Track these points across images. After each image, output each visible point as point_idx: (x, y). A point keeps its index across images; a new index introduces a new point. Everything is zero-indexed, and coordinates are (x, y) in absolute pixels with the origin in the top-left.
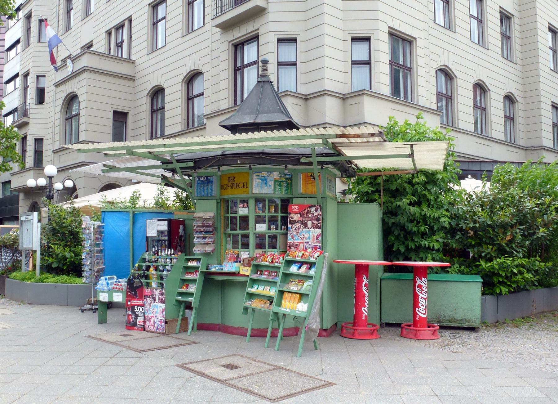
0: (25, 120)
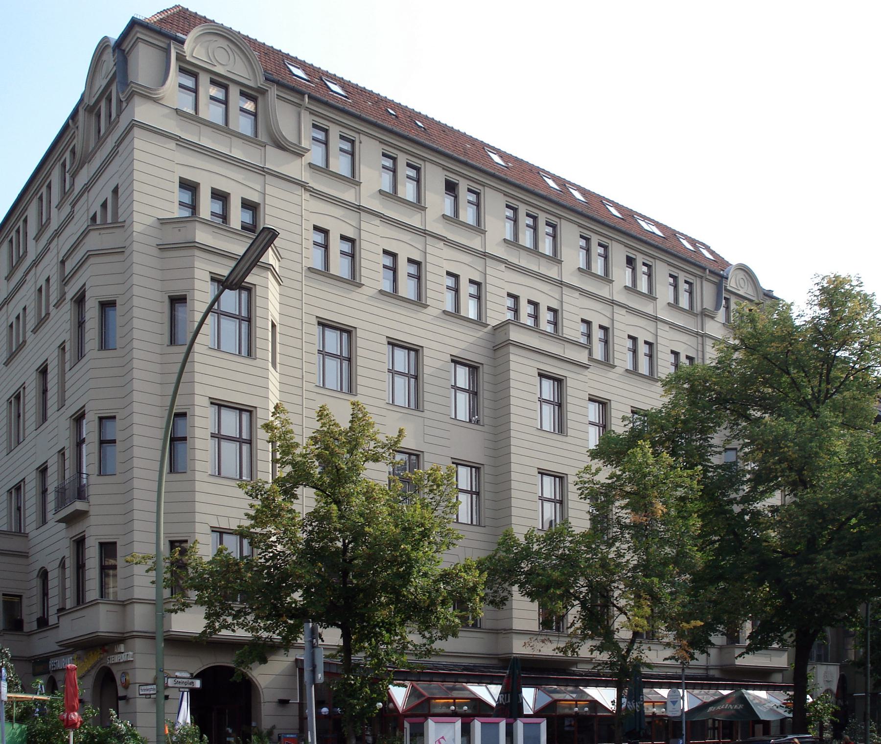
0: (79, 505)
